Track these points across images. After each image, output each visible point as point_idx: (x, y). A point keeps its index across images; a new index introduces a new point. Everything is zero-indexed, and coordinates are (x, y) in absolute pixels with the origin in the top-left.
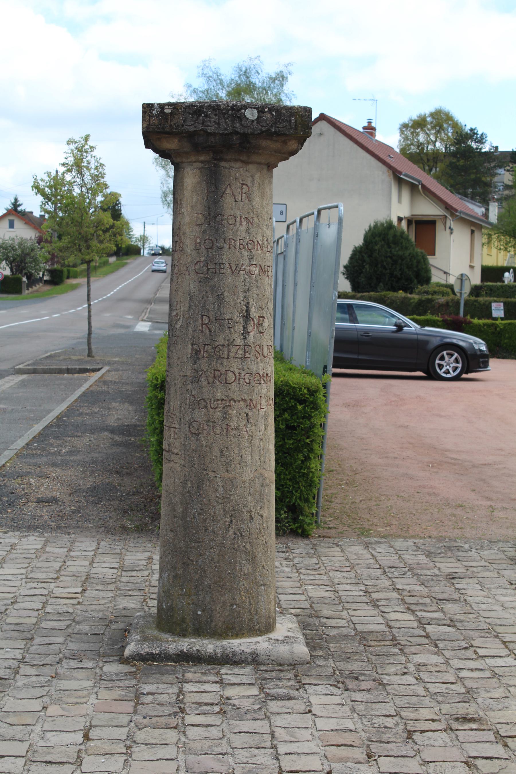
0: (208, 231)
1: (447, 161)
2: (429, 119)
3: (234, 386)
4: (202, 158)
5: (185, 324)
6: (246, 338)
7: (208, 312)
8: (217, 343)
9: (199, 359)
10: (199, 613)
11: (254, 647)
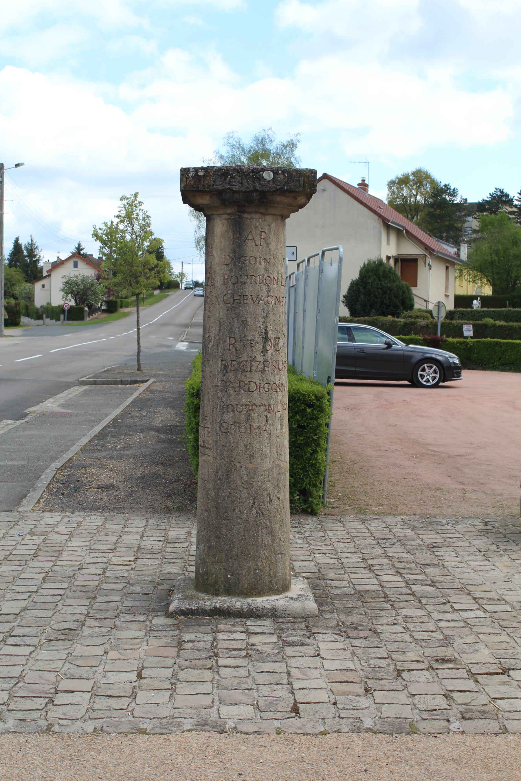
0: (234, 269)
1: (426, 211)
2: (411, 177)
3: (256, 394)
4: (229, 211)
5: (216, 344)
6: (265, 355)
8: (242, 360)
9: (227, 372)
10: (229, 576)
11: (273, 603)
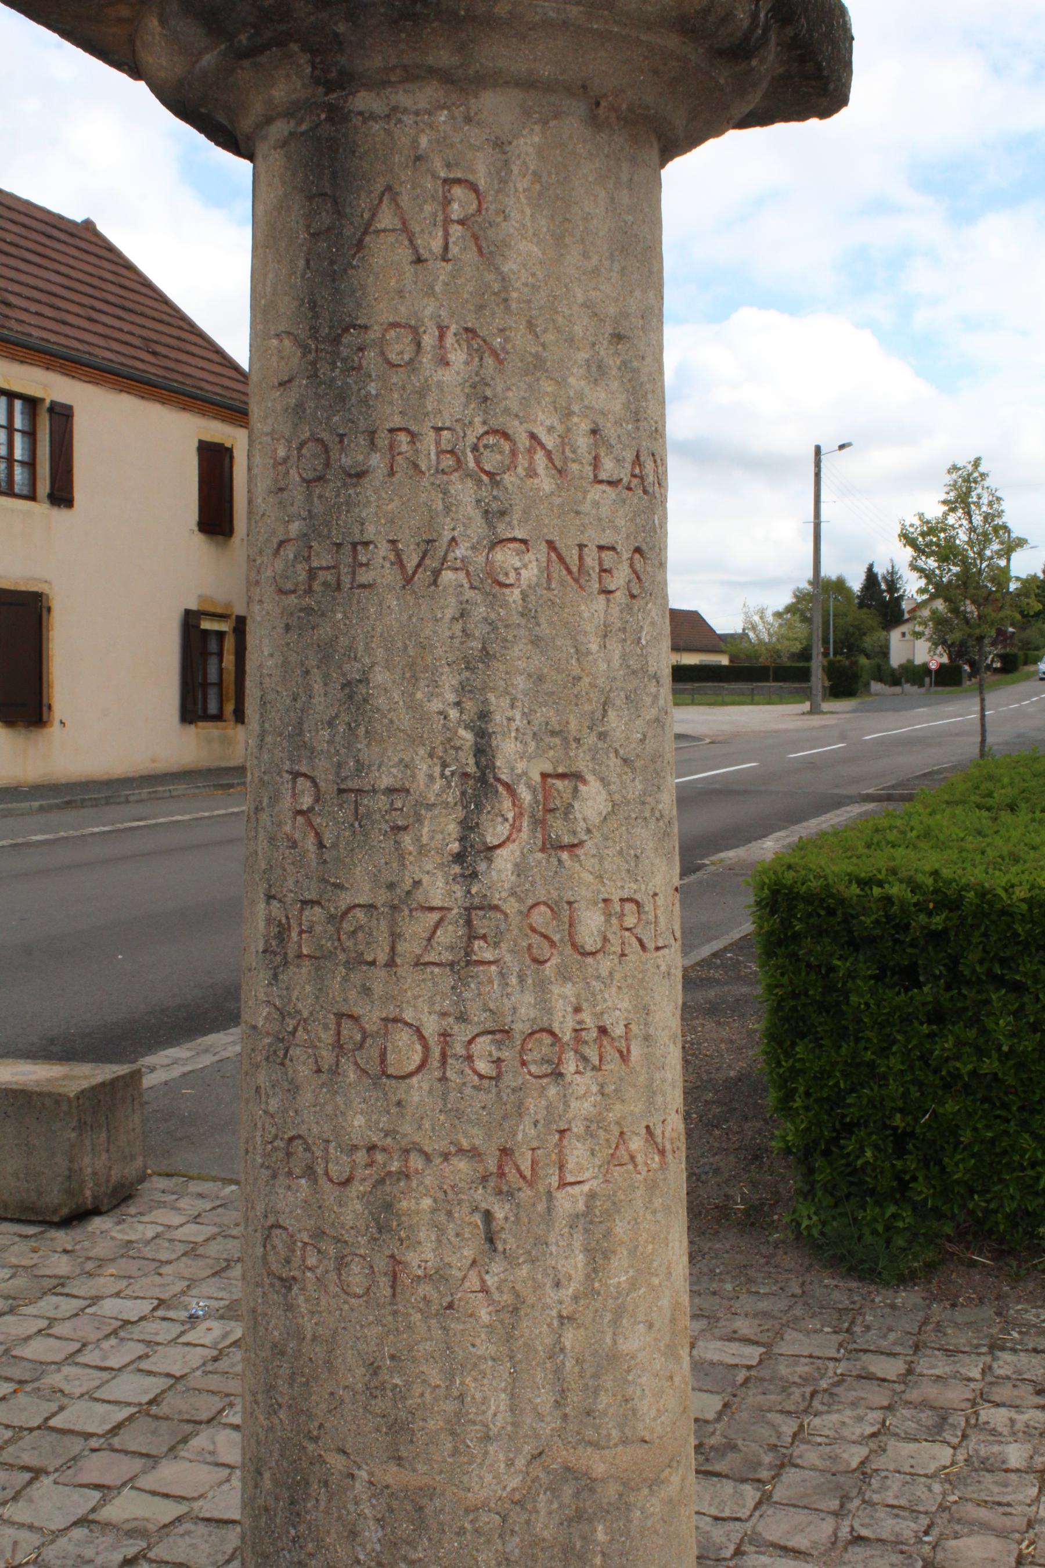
0: (311, 404)
3: (419, 1091)
6: (474, 875)
7: (311, 759)
8: (345, 900)
